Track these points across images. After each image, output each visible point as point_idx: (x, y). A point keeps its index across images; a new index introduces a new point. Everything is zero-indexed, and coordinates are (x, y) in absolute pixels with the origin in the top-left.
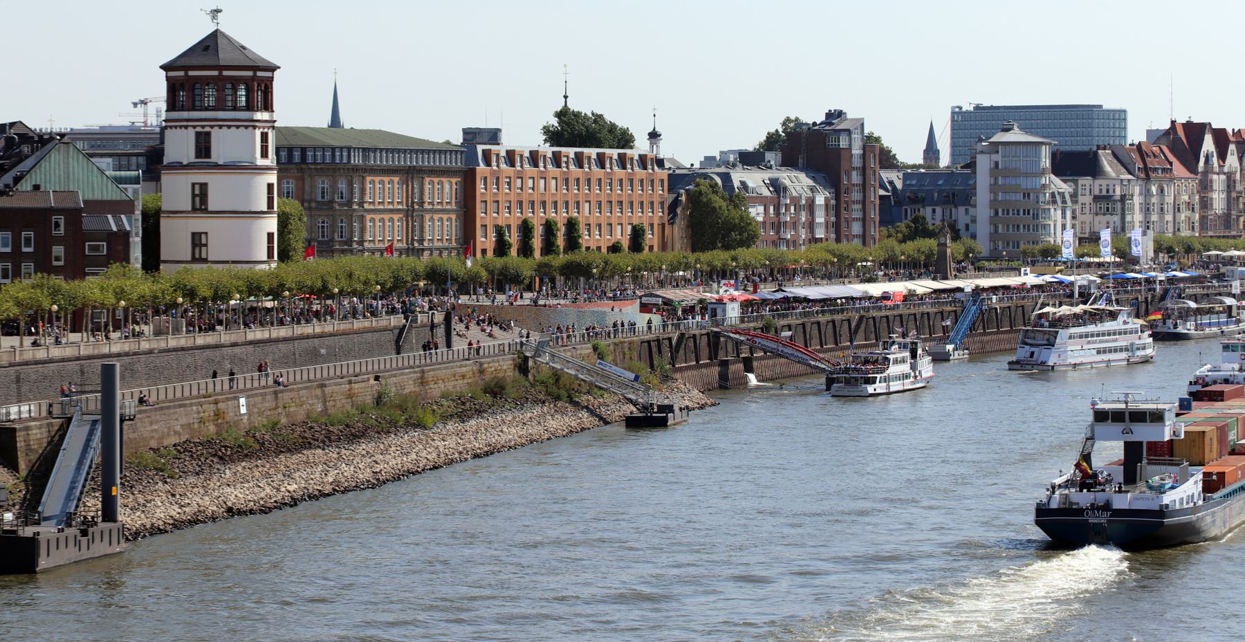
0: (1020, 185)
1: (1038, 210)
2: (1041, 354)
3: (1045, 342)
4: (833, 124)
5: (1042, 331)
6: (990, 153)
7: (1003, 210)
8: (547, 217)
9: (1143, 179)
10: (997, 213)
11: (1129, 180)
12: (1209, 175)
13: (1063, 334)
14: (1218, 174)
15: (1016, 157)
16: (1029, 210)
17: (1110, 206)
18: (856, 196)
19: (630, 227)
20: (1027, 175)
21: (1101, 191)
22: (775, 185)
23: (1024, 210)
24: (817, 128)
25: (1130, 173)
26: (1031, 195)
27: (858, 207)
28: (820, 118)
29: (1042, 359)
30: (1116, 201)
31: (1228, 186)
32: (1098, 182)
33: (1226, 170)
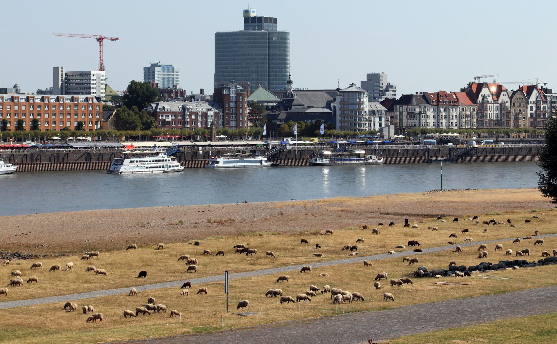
7: (350, 118)
8: (19, 118)
12: (485, 105)
26: (353, 111)
32: (409, 107)
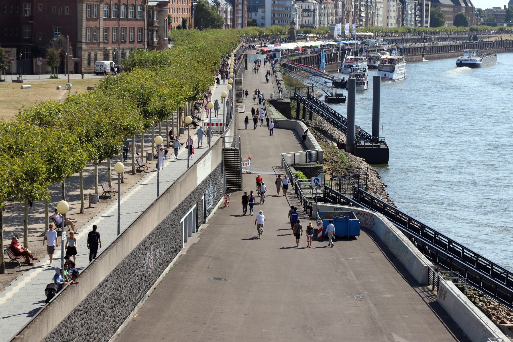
9: (319, 3)
10: (274, 15)
11: (315, 3)
13: (397, 66)
19: (181, 19)
21: (306, 8)
27: (240, 12)
29: (390, 77)
31: (342, 7)
32: (305, 4)
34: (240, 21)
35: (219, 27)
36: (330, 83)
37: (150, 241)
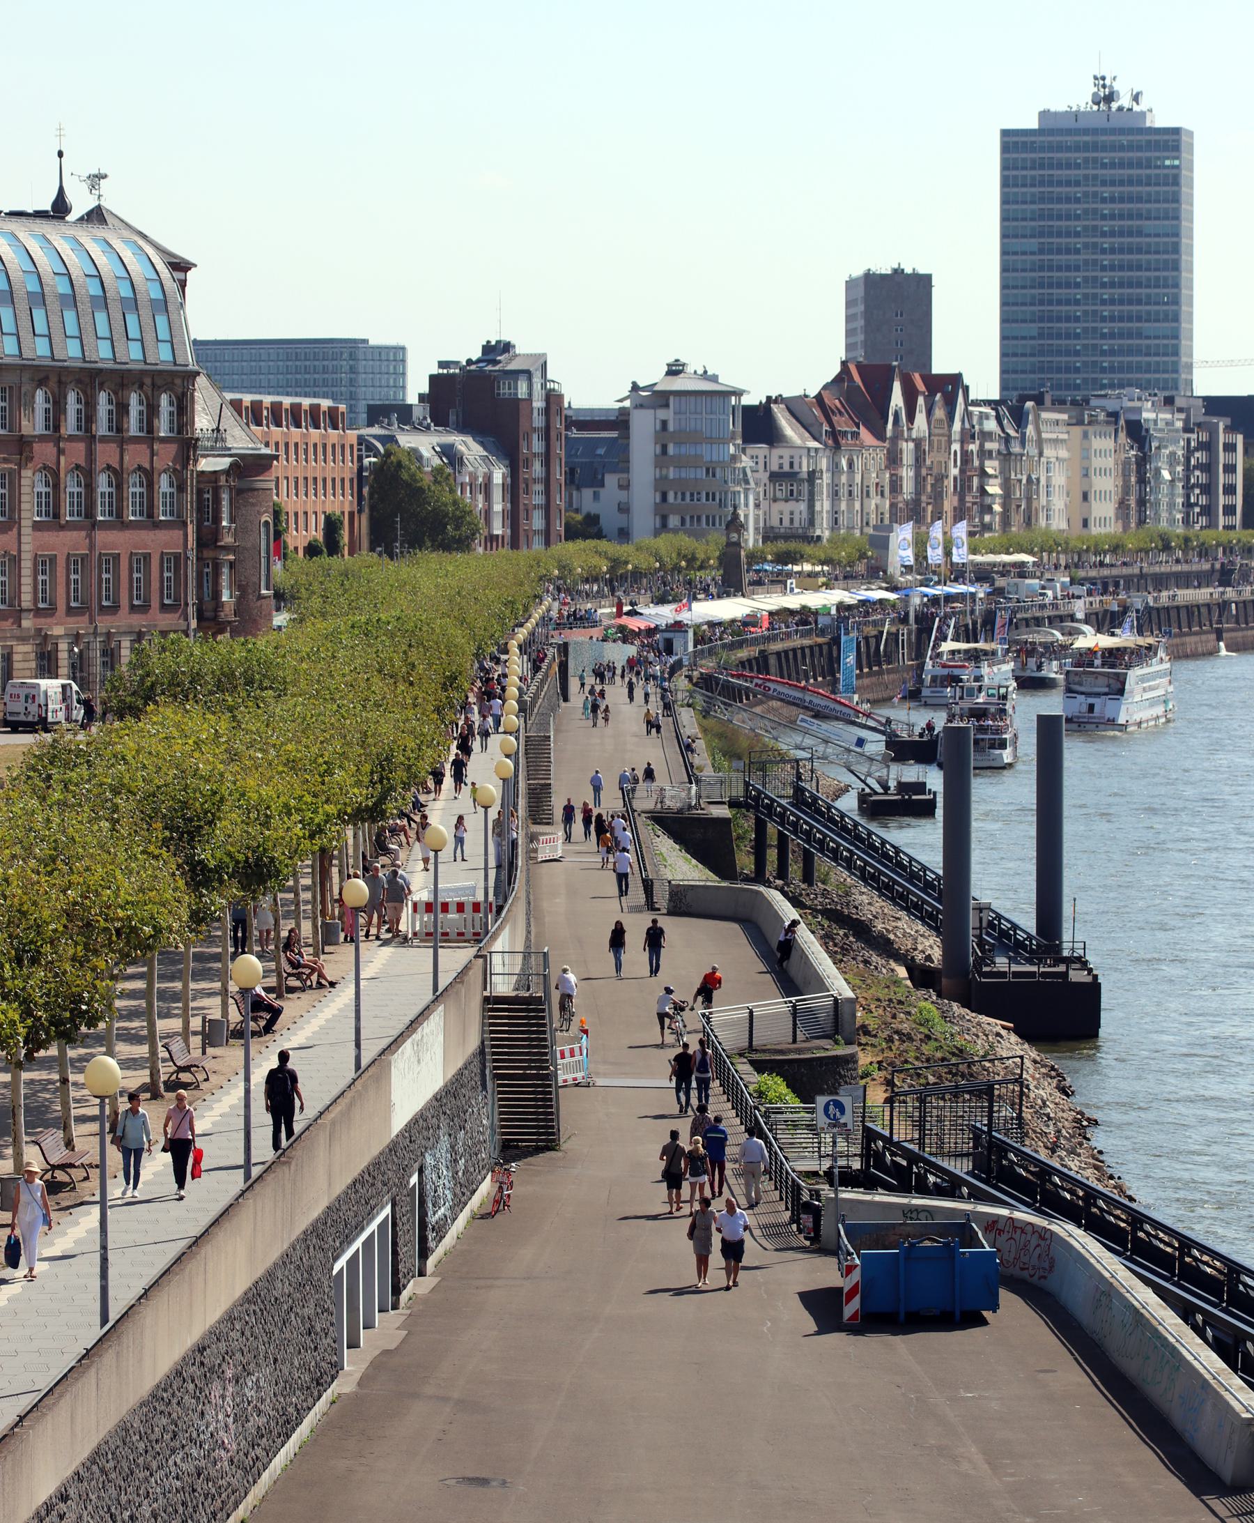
0: (702, 456)
1: (726, 493)
2: (1103, 706)
3: (1106, 690)
4: (499, 362)
5: (1094, 673)
6: (654, 407)
11: (816, 450)
13: (1134, 675)
14: (907, 441)
15: (696, 413)
16: (714, 494)
17: (795, 488)
18: (537, 468)
20: (711, 440)
21: (781, 466)
22: (448, 452)
23: (707, 494)
24: (473, 367)
25: (815, 439)
27: (539, 487)
28: (476, 354)
29: (1109, 715)
30: (803, 480)
31: (917, 460)
32: (776, 452)
33: (914, 436)
34: (538, 522)
35: (462, 544)
36: (876, 745)
37: (223, 1346)
